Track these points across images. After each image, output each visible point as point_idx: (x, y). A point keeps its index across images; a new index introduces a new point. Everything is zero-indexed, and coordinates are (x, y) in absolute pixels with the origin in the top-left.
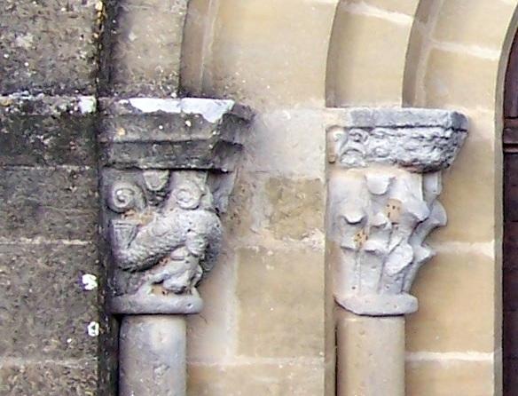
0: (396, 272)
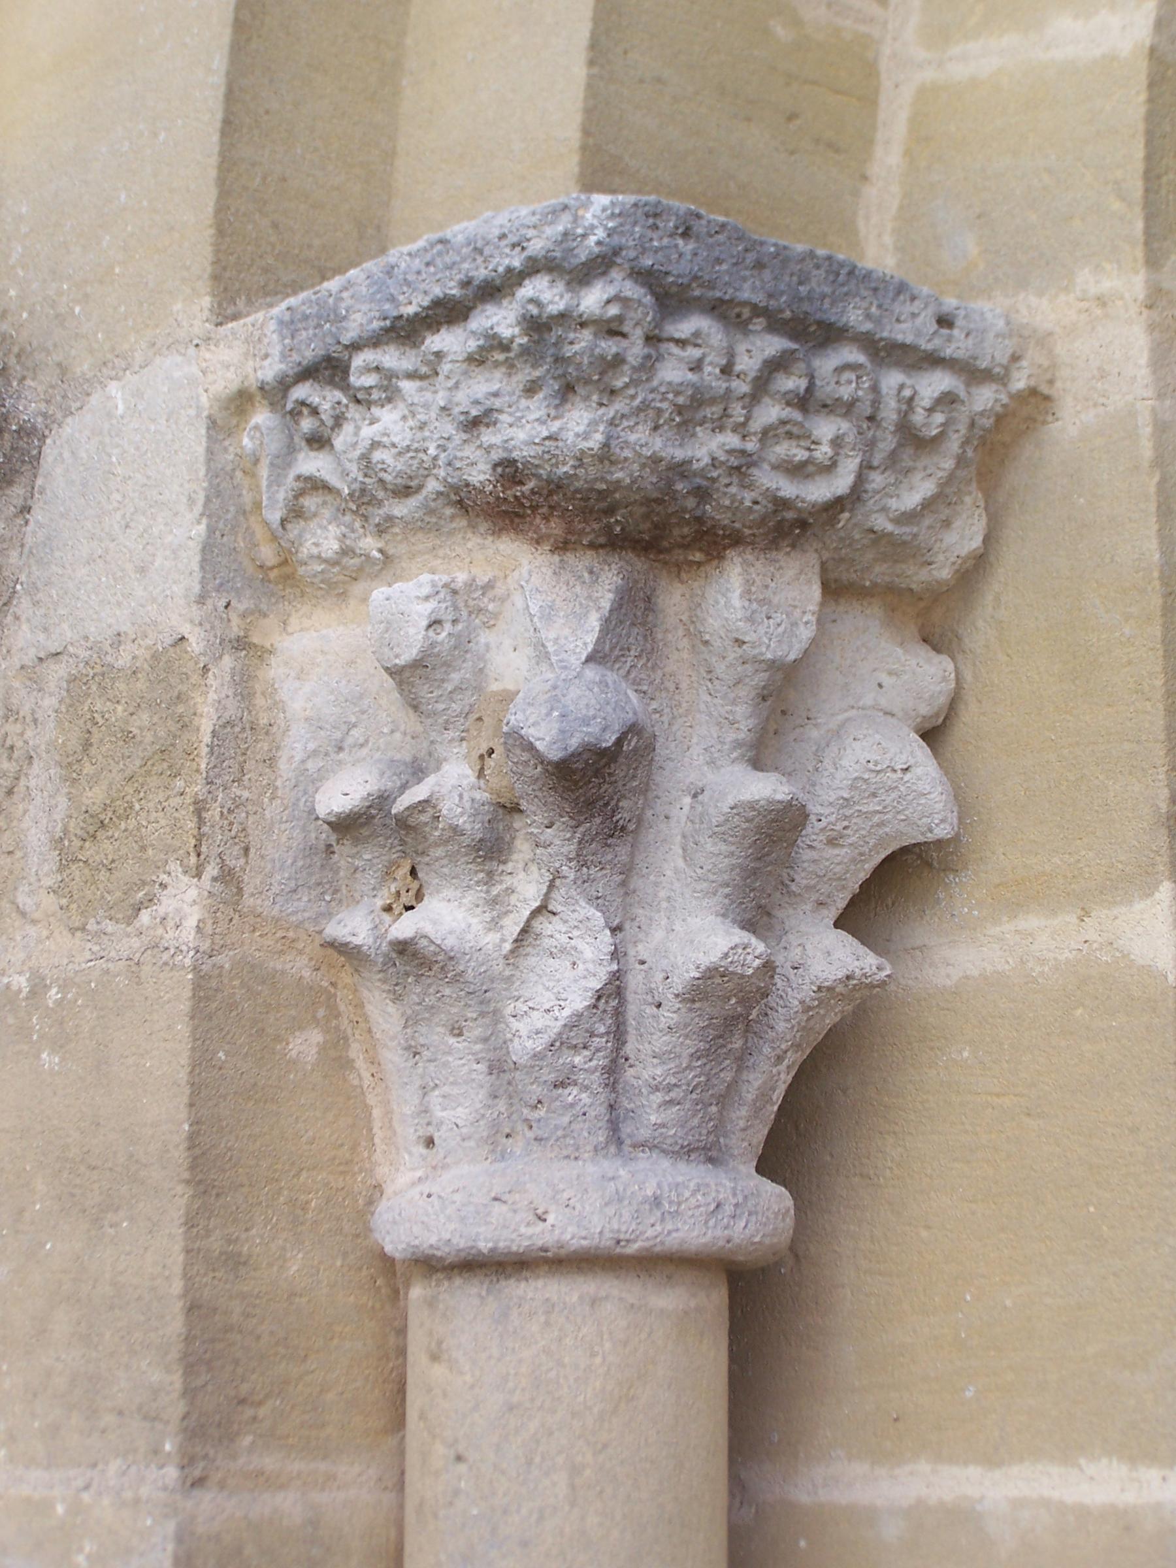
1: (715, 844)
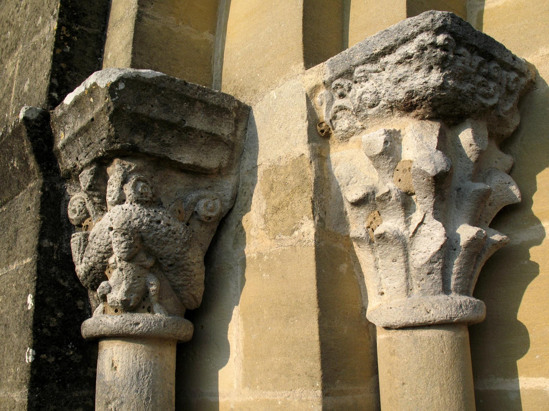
0: (424, 262)
1: (468, 203)
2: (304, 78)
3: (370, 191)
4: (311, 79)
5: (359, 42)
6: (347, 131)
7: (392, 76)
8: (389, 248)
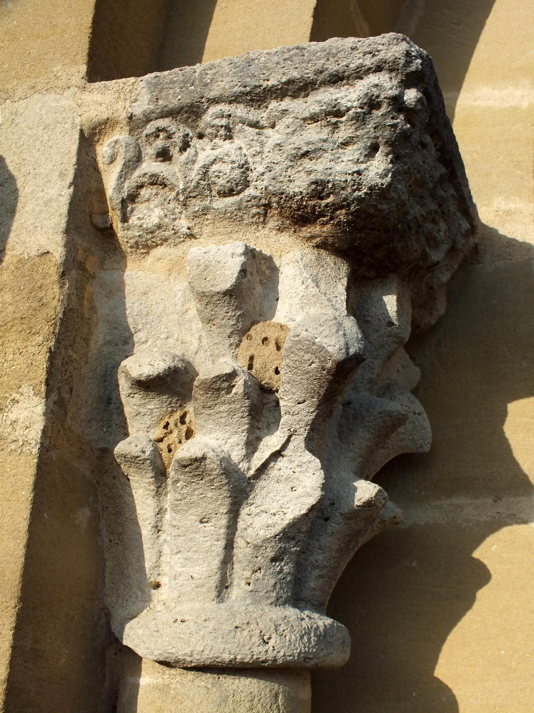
2: (83, 97)
3: (180, 365)
4: (101, 104)
5: (231, 57)
6: (152, 233)
7: (290, 141)
8: (201, 491)
